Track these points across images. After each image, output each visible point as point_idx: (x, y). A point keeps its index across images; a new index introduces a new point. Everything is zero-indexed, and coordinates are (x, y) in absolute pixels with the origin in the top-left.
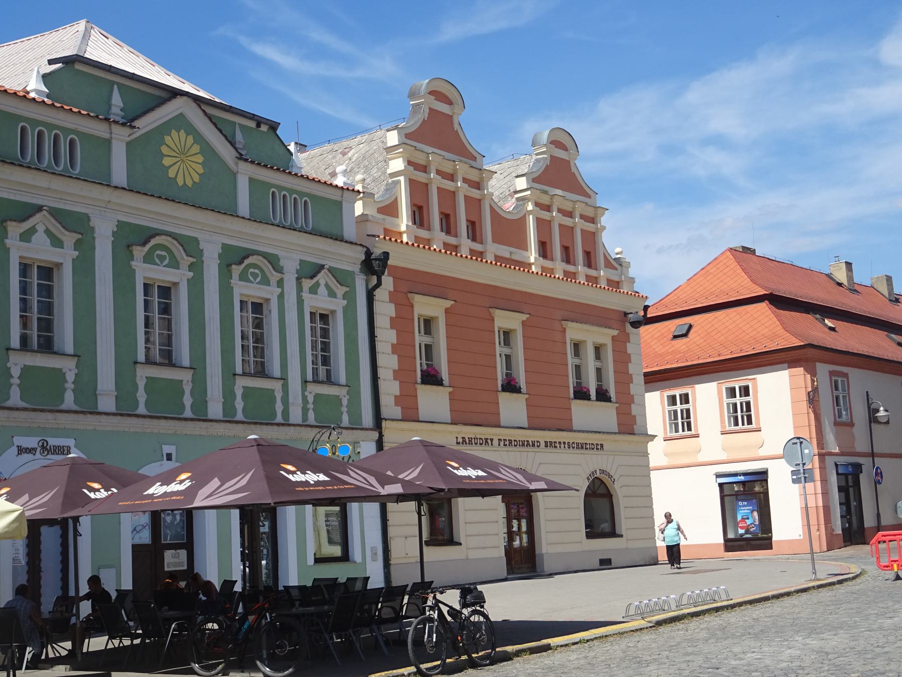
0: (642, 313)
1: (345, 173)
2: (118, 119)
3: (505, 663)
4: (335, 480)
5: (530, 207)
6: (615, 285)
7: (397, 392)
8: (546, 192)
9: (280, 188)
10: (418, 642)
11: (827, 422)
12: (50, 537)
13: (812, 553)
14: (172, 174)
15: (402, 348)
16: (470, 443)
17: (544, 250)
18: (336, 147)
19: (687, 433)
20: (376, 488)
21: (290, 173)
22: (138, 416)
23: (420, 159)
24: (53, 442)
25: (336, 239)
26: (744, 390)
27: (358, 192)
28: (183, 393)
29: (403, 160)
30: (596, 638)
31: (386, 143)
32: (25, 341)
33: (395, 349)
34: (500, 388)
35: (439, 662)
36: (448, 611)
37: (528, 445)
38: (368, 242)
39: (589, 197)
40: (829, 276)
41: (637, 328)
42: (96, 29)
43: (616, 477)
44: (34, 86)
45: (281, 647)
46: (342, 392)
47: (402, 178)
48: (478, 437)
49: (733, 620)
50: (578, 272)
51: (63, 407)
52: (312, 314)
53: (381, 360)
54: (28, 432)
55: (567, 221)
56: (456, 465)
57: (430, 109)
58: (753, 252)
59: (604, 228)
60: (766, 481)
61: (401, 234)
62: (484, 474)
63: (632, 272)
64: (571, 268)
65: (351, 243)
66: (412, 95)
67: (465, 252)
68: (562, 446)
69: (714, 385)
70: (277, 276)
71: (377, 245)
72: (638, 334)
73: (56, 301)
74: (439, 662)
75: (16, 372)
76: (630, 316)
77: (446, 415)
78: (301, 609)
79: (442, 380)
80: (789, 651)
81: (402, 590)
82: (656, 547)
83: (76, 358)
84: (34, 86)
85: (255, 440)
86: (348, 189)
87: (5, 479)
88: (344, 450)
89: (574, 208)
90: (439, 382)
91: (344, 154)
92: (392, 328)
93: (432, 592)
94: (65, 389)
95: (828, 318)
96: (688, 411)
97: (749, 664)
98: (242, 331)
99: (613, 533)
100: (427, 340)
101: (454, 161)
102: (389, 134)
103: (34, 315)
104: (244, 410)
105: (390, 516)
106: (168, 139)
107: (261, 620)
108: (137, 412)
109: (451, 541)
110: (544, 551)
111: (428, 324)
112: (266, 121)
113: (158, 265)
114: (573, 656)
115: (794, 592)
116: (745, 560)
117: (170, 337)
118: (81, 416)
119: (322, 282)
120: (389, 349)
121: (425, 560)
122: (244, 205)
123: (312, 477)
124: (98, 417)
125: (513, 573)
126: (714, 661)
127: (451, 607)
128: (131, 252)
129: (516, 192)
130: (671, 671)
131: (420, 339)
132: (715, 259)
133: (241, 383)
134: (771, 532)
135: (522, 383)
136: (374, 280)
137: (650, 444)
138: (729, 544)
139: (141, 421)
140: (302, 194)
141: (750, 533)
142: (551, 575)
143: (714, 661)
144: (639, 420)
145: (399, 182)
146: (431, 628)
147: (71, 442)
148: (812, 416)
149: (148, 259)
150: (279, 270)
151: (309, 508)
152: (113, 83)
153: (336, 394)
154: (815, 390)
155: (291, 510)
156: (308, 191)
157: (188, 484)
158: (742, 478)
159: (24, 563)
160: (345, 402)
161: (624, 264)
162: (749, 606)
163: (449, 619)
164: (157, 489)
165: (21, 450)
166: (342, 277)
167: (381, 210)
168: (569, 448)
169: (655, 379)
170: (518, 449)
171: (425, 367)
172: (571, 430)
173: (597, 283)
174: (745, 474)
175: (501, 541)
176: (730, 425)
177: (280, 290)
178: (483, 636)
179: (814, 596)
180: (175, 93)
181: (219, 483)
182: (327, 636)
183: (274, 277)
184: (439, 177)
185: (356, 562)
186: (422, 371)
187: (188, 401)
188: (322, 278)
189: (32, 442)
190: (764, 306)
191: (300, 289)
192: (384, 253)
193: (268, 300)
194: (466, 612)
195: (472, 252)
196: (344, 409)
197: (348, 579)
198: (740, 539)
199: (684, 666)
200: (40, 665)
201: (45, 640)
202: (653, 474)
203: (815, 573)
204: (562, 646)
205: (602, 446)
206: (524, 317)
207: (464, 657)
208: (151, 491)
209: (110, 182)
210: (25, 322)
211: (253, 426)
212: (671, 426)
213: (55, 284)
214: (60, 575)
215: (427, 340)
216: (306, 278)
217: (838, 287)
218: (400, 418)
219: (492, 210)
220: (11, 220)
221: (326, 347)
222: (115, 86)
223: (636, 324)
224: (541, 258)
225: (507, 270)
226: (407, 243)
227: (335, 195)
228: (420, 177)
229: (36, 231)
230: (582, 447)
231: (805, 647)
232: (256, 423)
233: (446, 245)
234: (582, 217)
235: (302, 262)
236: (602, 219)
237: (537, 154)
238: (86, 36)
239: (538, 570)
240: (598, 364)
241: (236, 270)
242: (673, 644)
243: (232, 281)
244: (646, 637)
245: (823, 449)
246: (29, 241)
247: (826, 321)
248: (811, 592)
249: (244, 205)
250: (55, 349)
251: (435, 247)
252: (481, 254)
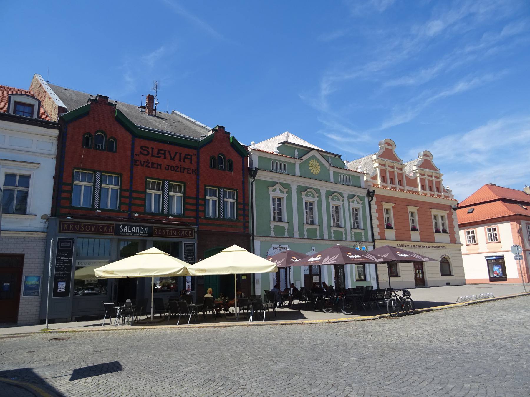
0: (457, 206)
1: (361, 168)
2: (297, 157)
3: (418, 314)
4: (363, 257)
5: (418, 175)
6: (447, 197)
7: (379, 231)
8: (423, 170)
9: (342, 174)
10: (390, 306)
11: (525, 240)
12: (282, 271)
13: (523, 283)
14: (312, 171)
15: (380, 218)
16: (402, 246)
17: (423, 187)
18: (357, 161)
19: (474, 243)
21: (345, 169)
22: (305, 239)
23: (383, 163)
24: (282, 246)
25: (359, 187)
27: (365, 173)
29: (378, 163)
30: (448, 308)
31: (372, 159)
32: (274, 218)
33: (378, 218)
34: (411, 230)
35: (397, 313)
36: (399, 297)
37: (421, 247)
38: (368, 188)
39: (437, 171)
40: (523, 192)
41: (455, 210)
42: (290, 134)
43: (450, 257)
44: (275, 151)
45: (348, 306)
47: (378, 169)
48: (405, 244)
49: (496, 304)
50: (435, 194)
51: (285, 236)
52: (353, 209)
53: (373, 222)
54: (276, 243)
55: (430, 179)
56: (399, 253)
57: (386, 148)
58: (495, 185)
59: (443, 180)
60: (504, 259)
61: (378, 185)
62: (409, 256)
63: (453, 193)
64: (432, 193)
65: (363, 188)
66: (380, 144)
67: (398, 189)
68: (432, 247)
69: (483, 228)
70: (342, 198)
71: (371, 188)
72: (456, 212)
73: (282, 208)
74: (397, 313)
75: (272, 227)
76: (453, 207)
77: (394, 238)
78: (354, 295)
79: (392, 227)
80: (519, 316)
81: (384, 290)
82: (465, 280)
83: (288, 223)
84: (275, 151)
85: (339, 245)
86: (362, 173)
87: (270, 256)
88: (363, 248)
89: (425, 173)
90: (391, 228)
91: (360, 163)
92: (376, 212)
93: (394, 291)
94: (285, 232)
95: (524, 205)
96: (474, 236)
97: (504, 320)
98: (333, 214)
99: (450, 275)
100: (387, 216)
101: (393, 163)
102: (373, 156)
103: (277, 211)
104: (334, 237)
105: (378, 268)
106: (310, 162)
107: (342, 298)
108: (305, 238)
109: (397, 276)
110: (427, 280)
111: (387, 211)
113: (309, 197)
114: (441, 313)
115: (518, 296)
116: (498, 285)
117: (313, 216)
118: (290, 239)
119: (355, 200)
120: (376, 219)
121: (391, 281)
122: (332, 179)
123: (356, 256)
124: (294, 239)
125: (418, 286)
126: (491, 318)
127: (400, 296)
128: (301, 193)
129: (413, 171)
130: (476, 320)
131: (385, 215)
132: (481, 188)
133: (333, 229)
134: (506, 276)
135: (418, 228)
136: (371, 199)
137: (462, 247)
138: (491, 279)
139: (305, 240)
140: (348, 175)
141: (499, 276)
142: (430, 287)
143: (491, 318)
144: (457, 239)
145: (377, 170)
146: (394, 302)
147: (287, 246)
148: (520, 237)
149: (306, 195)
150: (343, 197)
151: (354, 265)
152: (295, 148)
153: (360, 232)
154: (521, 229)
155: (348, 265)
156: (350, 174)
157: (320, 258)
158: (495, 258)
159: (276, 279)
160: (363, 234)
161: (450, 191)
162: (501, 300)
163: (399, 300)
164: (312, 259)
165: (274, 248)
166: (360, 197)
167: (372, 178)
168: (434, 248)
169: (462, 226)
170: (417, 248)
171: (387, 224)
172: (434, 242)
173: (441, 197)
174: (496, 257)
175: (413, 277)
176: (489, 241)
177: (343, 202)
178: (410, 305)
179: (525, 297)
180: (312, 149)
181: (329, 258)
182: (362, 303)
183: (341, 199)
184: (389, 168)
185: (368, 281)
186: (386, 225)
187: (318, 234)
188: (355, 198)
189: (277, 246)
190: (500, 202)
191: (349, 202)
192: (373, 191)
193: (340, 205)
194: (405, 298)
195: (400, 189)
196: (363, 236)
197: (367, 286)
198: (495, 277)
199: (480, 319)
200: (281, 307)
201: (282, 300)
202: (463, 256)
203: (525, 290)
204: (436, 310)
205: (445, 247)
206: (418, 208)
207: (405, 312)
208: (310, 260)
209: (295, 174)
210: (274, 213)
211: (337, 241)
212: (468, 241)
213: (282, 203)
214: (285, 282)
215: (387, 216)
216: (350, 199)
217: (527, 195)
218: (380, 239)
219: (406, 176)
220: (270, 186)
221: (357, 219)
222: (296, 149)
223: (455, 209)
224: (422, 190)
225: (410, 194)
226: (380, 187)
227: (358, 175)
228: (383, 168)
229: (276, 189)
230: (438, 248)
231: (525, 315)
232: (337, 241)
233: (392, 188)
234: (435, 177)
235: (349, 194)
236: (442, 177)
237: (419, 159)
238: (288, 136)
239: (426, 285)
240: (443, 222)
241: (330, 197)
242: (475, 311)
243: (302, 197)
244: (465, 308)
245: (524, 248)
246: (275, 192)
247: (523, 206)
248: (524, 296)
249: (332, 179)
250: (282, 221)
251: (389, 188)
252: (403, 190)
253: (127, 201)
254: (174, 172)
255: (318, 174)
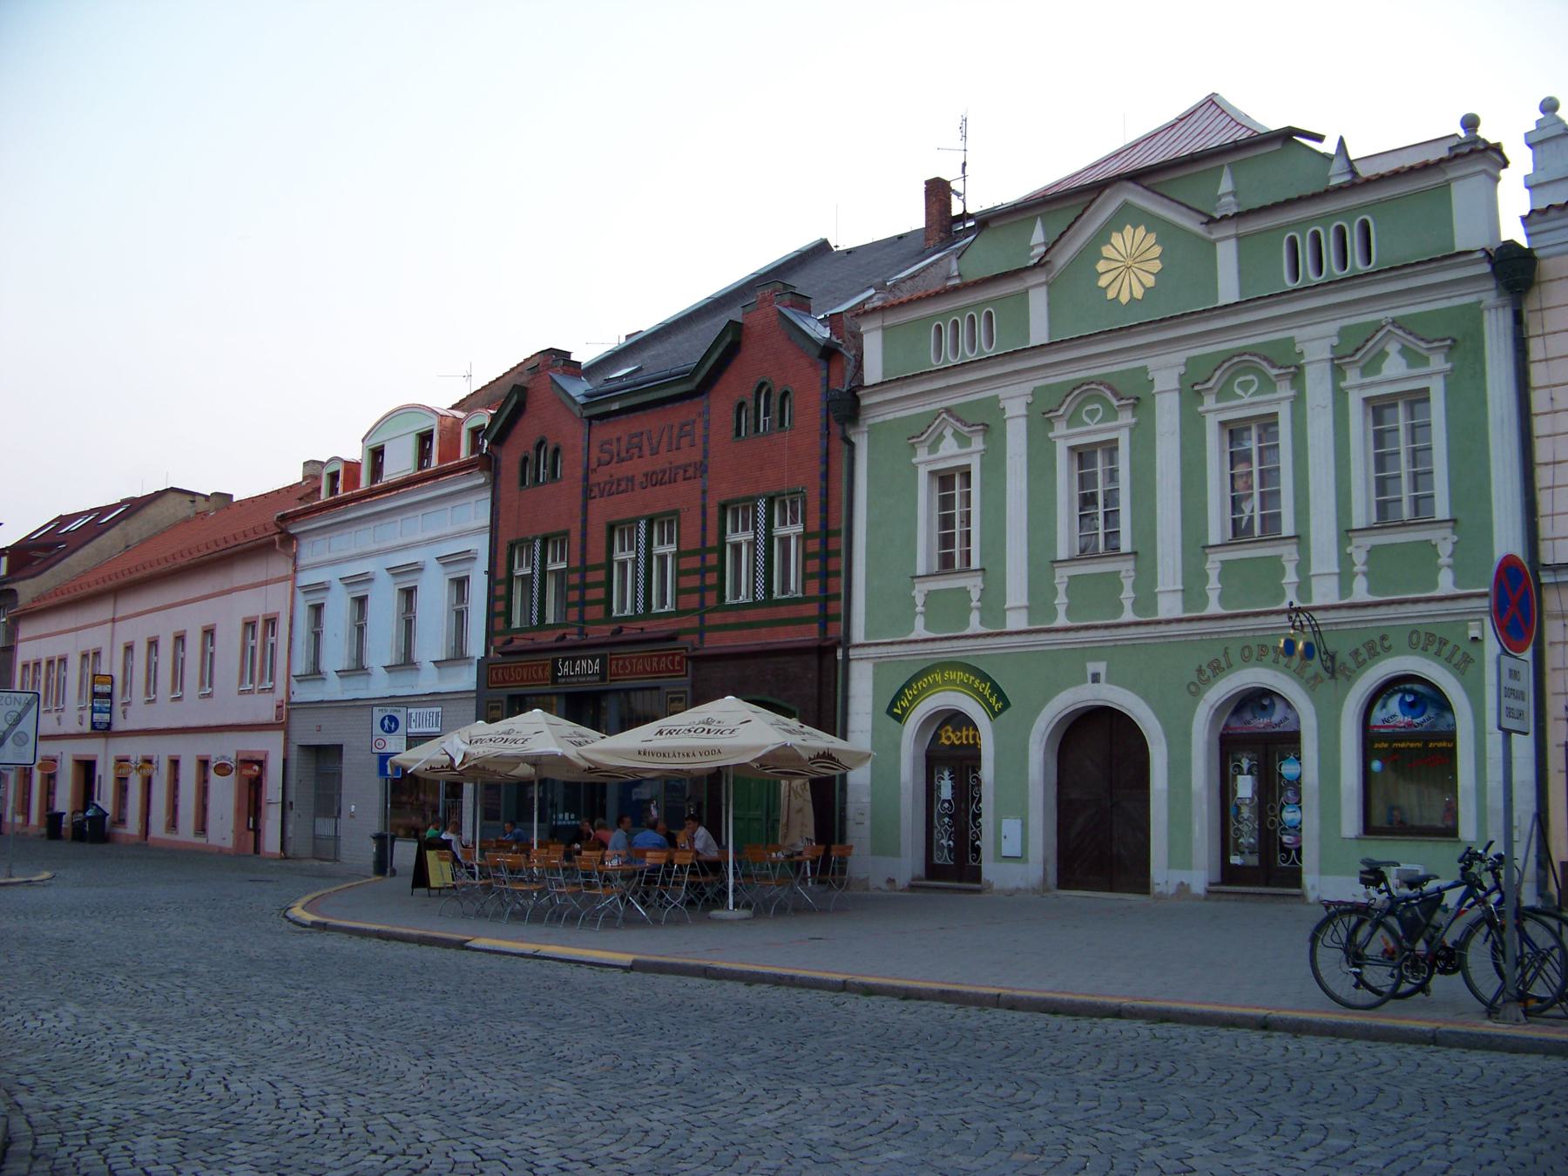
20: (784, 730)
26: (1398, 441)
28: (1121, 588)
46: (1126, 568)
75: (920, 600)
112: (901, 268)
253: (574, 596)
254: (658, 487)
255: (1132, 299)
